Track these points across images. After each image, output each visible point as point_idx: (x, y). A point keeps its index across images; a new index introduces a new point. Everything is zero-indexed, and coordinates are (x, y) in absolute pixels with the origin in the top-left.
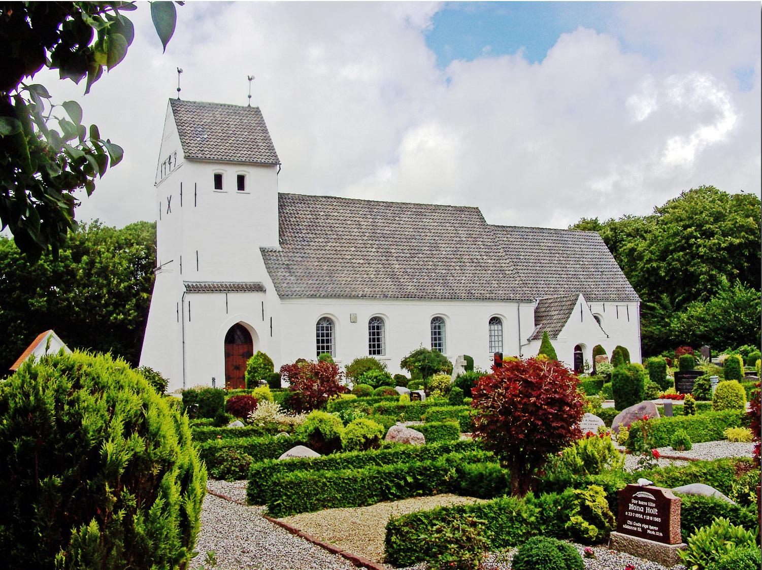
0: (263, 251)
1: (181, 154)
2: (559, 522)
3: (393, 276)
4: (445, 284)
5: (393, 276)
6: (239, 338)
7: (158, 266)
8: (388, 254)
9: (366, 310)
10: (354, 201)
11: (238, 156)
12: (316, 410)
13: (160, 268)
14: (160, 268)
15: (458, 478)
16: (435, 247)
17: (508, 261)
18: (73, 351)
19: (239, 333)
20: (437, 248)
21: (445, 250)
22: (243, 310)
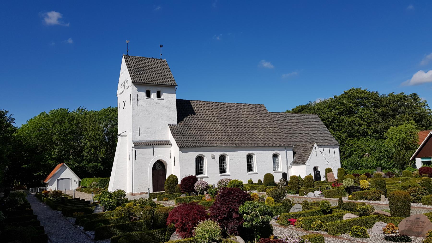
0: (170, 125)
1: (130, 81)
2: (179, 187)
3: (229, 136)
4: (252, 139)
5: (229, 136)
6: (159, 168)
7: (119, 133)
8: (226, 126)
9: (217, 154)
10: (209, 103)
11: (157, 82)
12: (71, 110)
13: (120, 135)
14: (120, 135)
15: (242, 224)
16: (246, 122)
17: (279, 128)
18: (299, 176)
19: (159, 164)
20: (247, 123)
21: (251, 124)
22: (161, 154)
